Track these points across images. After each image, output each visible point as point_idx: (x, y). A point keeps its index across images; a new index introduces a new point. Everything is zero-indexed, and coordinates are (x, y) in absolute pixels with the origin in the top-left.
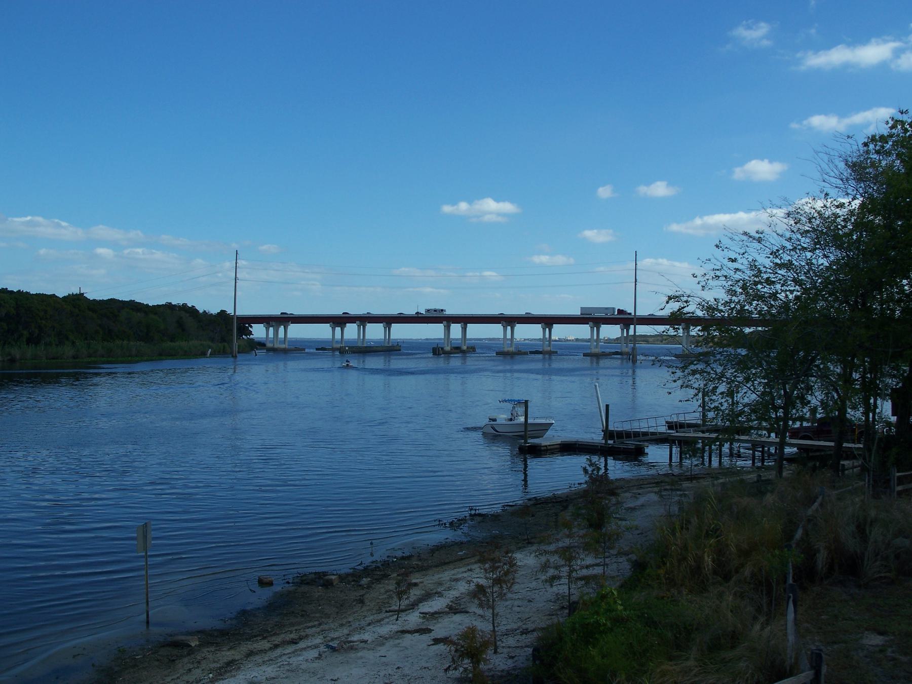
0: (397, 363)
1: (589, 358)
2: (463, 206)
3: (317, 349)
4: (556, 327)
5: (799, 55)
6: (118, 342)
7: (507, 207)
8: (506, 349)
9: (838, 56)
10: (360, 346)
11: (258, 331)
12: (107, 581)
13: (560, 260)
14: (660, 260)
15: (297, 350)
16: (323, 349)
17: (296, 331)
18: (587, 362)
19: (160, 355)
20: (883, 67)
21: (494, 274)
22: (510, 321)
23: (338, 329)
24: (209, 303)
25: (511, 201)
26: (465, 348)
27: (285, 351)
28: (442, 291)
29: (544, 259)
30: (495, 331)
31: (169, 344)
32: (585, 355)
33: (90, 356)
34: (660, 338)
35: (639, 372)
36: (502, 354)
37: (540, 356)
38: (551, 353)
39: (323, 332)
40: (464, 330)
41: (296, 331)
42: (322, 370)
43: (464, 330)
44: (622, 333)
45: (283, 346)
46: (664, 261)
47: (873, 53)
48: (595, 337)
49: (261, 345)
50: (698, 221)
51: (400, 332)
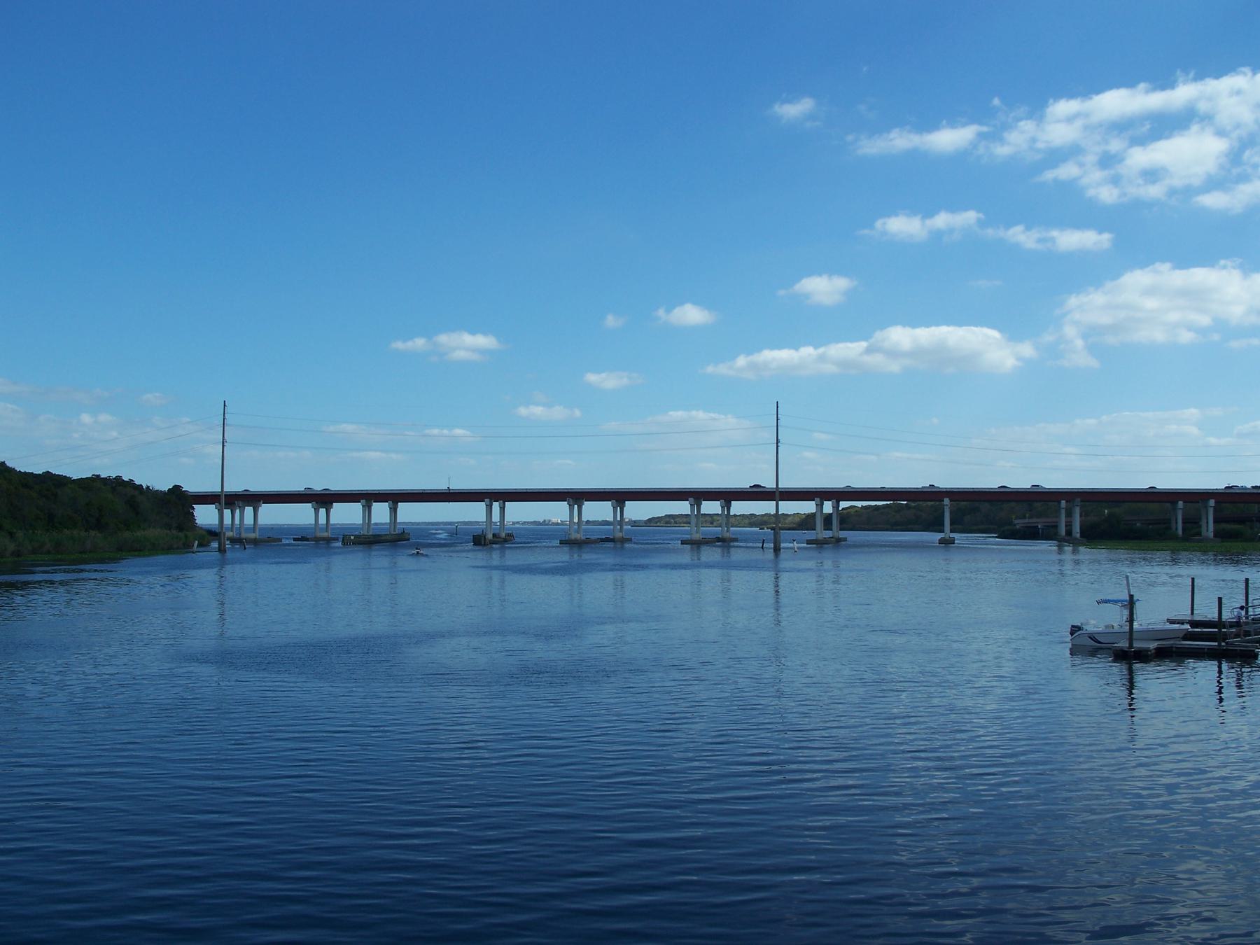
0: (514, 557)
1: (688, 547)
2: (420, 342)
3: (295, 539)
4: (629, 505)
5: (850, 138)
6: (66, 532)
7: (483, 341)
8: (574, 536)
9: (900, 141)
10: (378, 532)
11: (205, 515)
12: (688, 874)
13: (558, 413)
14: (694, 413)
15: (268, 543)
16: (303, 539)
17: (271, 515)
18: (563, 556)
19: (120, 549)
20: (959, 159)
21: (468, 433)
22: (324, 499)
23: (322, 511)
24: (156, 477)
25: (485, 333)
26: (503, 535)
27: (255, 542)
28: (394, 456)
29: (538, 410)
30: (557, 512)
31: (127, 534)
32: (683, 542)
33: (34, 552)
34: (708, 518)
35: (786, 561)
36: (568, 542)
37: (611, 545)
38: (624, 541)
39: (302, 515)
40: (394, 510)
41: (271, 515)
42: (674, 567)
43: (394, 510)
44: (692, 510)
45: (252, 536)
46: (701, 415)
47: (949, 139)
48: (576, 520)
49: (213, 534)
50: (741, 361)
51: (410, 513)
